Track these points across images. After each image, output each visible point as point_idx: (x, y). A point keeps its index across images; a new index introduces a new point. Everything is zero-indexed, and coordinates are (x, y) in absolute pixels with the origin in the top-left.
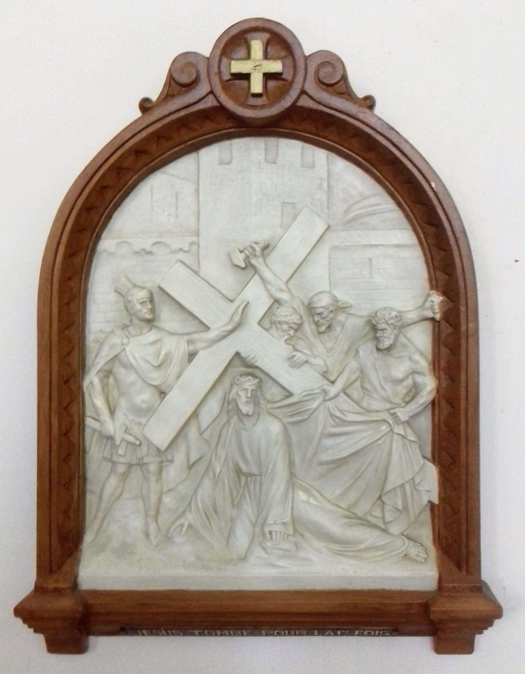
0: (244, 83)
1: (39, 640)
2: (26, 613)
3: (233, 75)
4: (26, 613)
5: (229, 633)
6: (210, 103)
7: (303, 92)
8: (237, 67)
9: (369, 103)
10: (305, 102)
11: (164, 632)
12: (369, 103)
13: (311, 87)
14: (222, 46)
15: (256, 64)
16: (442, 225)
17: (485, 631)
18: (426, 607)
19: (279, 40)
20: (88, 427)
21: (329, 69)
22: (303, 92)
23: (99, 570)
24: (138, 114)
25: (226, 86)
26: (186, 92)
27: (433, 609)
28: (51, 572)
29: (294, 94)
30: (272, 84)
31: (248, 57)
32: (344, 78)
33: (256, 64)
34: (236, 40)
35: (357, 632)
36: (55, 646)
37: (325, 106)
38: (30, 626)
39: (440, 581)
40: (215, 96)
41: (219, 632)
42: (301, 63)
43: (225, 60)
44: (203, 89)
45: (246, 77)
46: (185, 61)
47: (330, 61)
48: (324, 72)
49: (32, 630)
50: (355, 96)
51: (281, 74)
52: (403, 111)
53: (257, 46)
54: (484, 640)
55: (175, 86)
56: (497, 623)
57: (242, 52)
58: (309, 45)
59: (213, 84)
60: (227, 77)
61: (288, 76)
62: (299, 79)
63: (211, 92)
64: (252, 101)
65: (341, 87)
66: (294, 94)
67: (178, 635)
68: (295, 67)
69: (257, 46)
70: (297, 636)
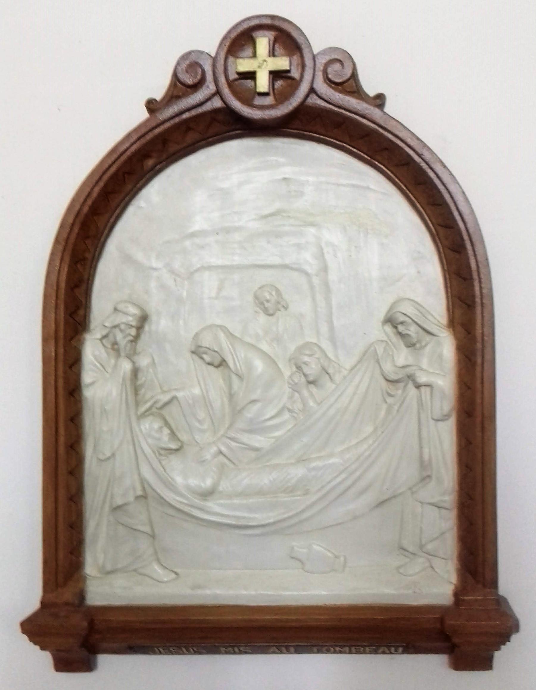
0: (249, 83)
1: (45, 658)
2: (35, 629)
3: (239, 74)
4: (35, 629)
5: (240, 650)
6: (217, 103)
7: (312, 90)
8: (244, 65)
9: (379, 100)
10: (313, 100)
11: (184, 649)
12: (379, 100)
13: (321, 86)
14: (228, 43)
15: (263, 62)
16: (457, 225)
17: (502, 647)
18: (442, 620)
19: (286, 38)
20: (283, 55)
21: (337, 66)
22: (312, 90)
23: (107, 585)
24: (144, 115)
25: (230, 84)
26: (192, 93)
27: (451, 622)
28: (57, 586)
29: (304, 88)
30: (279, 84)
31: (254, 55)
32: (354, 76)
33: (263, 62)
34: (241, 39)
35: (324, 649)
36: (64, 664)
37: (334, 105)
38: (35, 643)
39: (457, 594)
40: (223, 100)
41: (223, 649)
42: (309, 63)
43: (231, 59)
44: (210, 88)
45: (251, 75)
46: (191, 62)
47: (340, 58)
48: (334, 71)
49: (37, 648)
50: (367, 95)
51: (288, 71)
52: (414, 110)
53: (263, 43)
54: (500, 656)
55: (179, 88)
56: (514, 638)
57: (249, 51)
58: (319, 38)
59: (220, 85)
60: (233, 76)
61: (295, 74)
62: (308, 77)
63: (218, 93)
64: (258, 101)
65: (351, 86)
66: (304, 88)
67: (246, 653)
68: (303, 66)
69: (263, 43)
70: (338, 653)
